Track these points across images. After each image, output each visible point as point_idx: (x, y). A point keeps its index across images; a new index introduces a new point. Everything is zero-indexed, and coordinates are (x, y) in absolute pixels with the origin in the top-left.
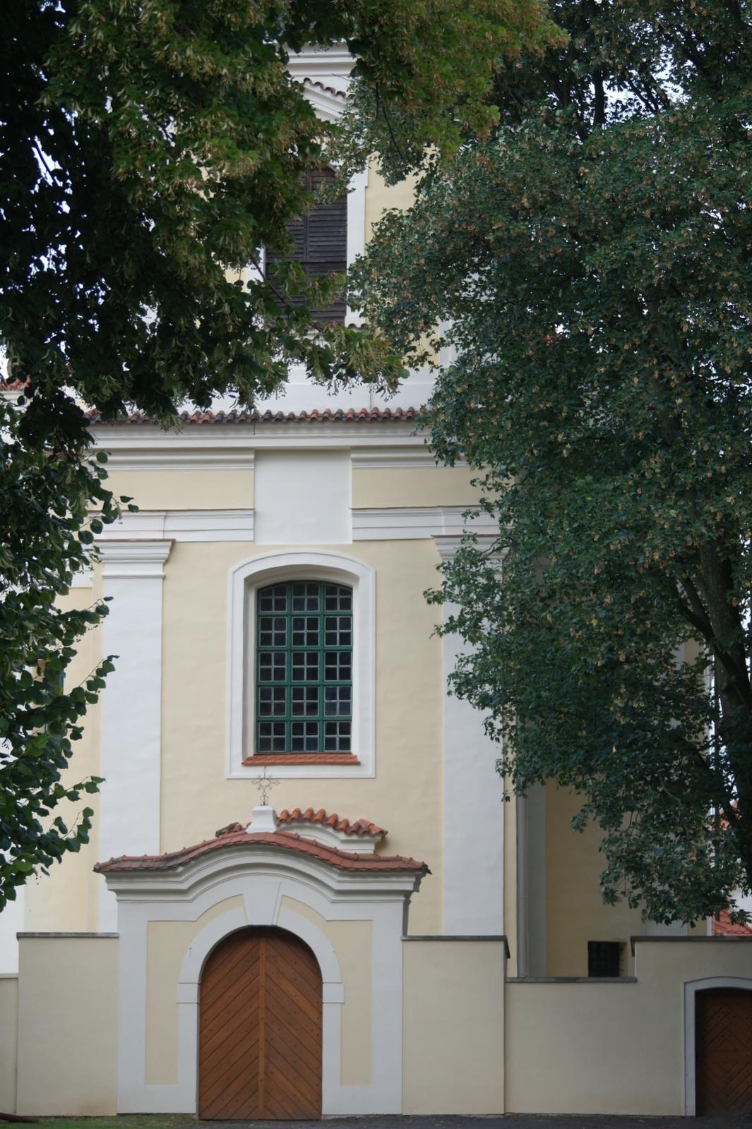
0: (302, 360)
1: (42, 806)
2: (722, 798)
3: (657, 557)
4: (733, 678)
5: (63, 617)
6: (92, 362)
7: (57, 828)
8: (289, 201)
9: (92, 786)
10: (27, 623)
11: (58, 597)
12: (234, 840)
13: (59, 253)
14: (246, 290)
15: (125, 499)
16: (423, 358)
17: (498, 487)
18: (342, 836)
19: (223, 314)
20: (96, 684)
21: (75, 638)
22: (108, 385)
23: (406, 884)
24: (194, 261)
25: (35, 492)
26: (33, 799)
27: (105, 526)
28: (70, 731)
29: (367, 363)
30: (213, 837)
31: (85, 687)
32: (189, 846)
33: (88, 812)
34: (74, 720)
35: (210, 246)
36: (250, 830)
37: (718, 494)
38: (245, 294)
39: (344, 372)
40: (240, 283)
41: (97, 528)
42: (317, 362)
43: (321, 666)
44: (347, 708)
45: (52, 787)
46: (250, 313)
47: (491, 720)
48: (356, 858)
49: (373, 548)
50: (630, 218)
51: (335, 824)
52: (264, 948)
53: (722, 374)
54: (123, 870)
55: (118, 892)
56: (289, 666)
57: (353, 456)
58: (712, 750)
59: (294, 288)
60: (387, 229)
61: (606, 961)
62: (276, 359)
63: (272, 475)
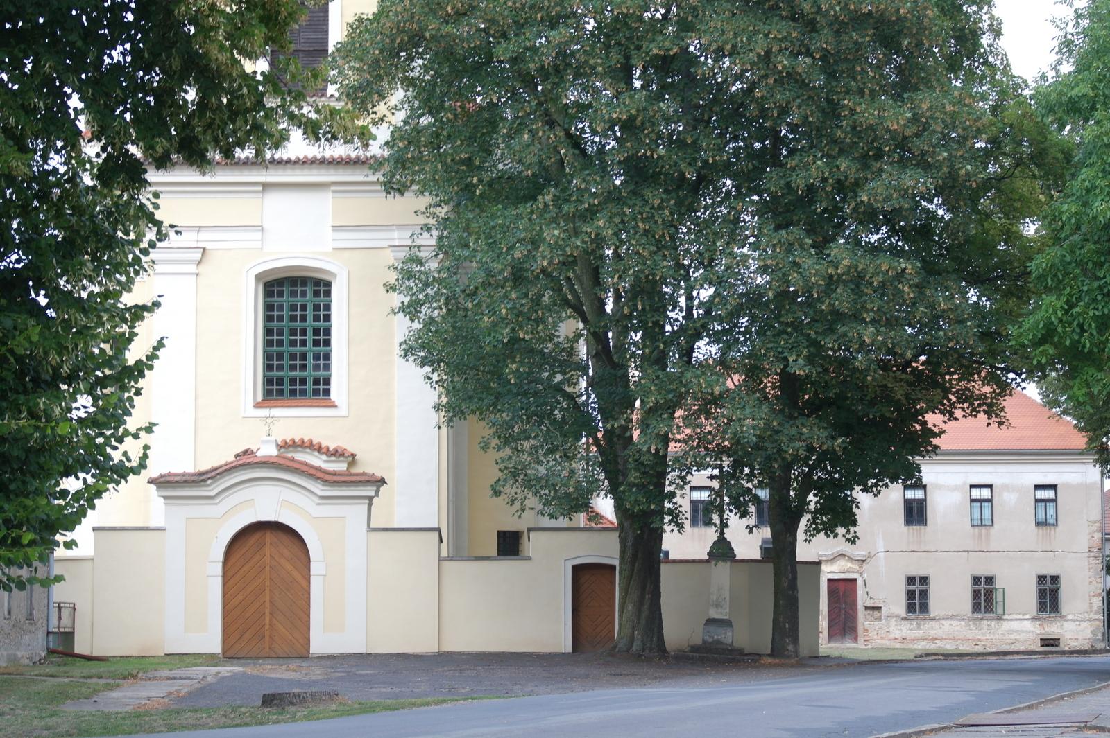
0: (300, 127)
1: (114, 443)
2: (592, 433)
3: (545, 264)
4: (600, 347)
5: (128, 309)
6: (150, 125)
7: (124, 459)
8: (290, 14)
9: (149, 430)
10: (102, 314)
11: (125, 294)
12: (248, 461)
13: (125, 49)
14: (259, 77)
15: (172, 226)
16: (382, 120)
17: (434, 215)
18: (324, 457)
19: (243, 95)
20: (152, 357)
21: (137, 324)
22: (161, 144)
23: (369, 491)
24: (222, 57)
25: (108, 220)
26: (107, 438)
27: (159, 244)
28: (133, 390)
29: (346, 130)
30: (232, 458)
31: (145, 360)
32: (216, 465)
33: (146, 447)
34: (136, 382)
35: (233, 46)
36: (258, 454)
37: (592, 220)
38: (258, 81)
39: (330, 136)
40: (255, 72)
41: (152, 245)
42: (310, 130)
43: (310, 337)
44: (327, 367)
45: (121, 430)
46: (263, 94)
47: (430, 375)
48: (335, 474)
49: (347, 254)
50: (526, 22)
51: (319, 449)
52: (269, 537)
53: (595, 133)
54: (168, 482)
55: (165, 498)
56: (286, 337)
57: (333, 188)
58: (584, 398)
59: (293, 77)
60: (357, 28)
61: (509, 544)
62: (281, 127)
63: (275, 201)
